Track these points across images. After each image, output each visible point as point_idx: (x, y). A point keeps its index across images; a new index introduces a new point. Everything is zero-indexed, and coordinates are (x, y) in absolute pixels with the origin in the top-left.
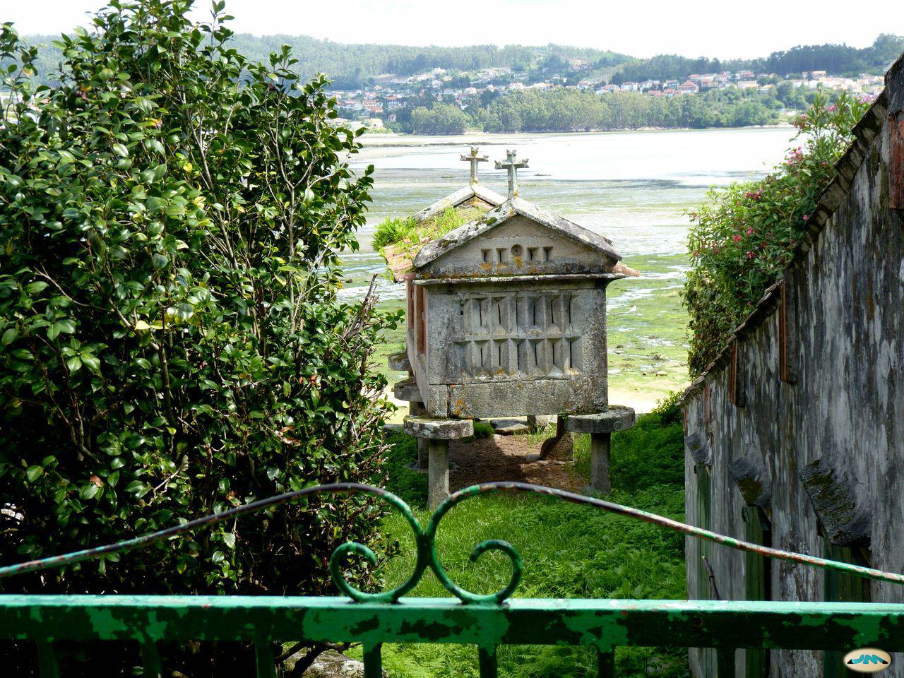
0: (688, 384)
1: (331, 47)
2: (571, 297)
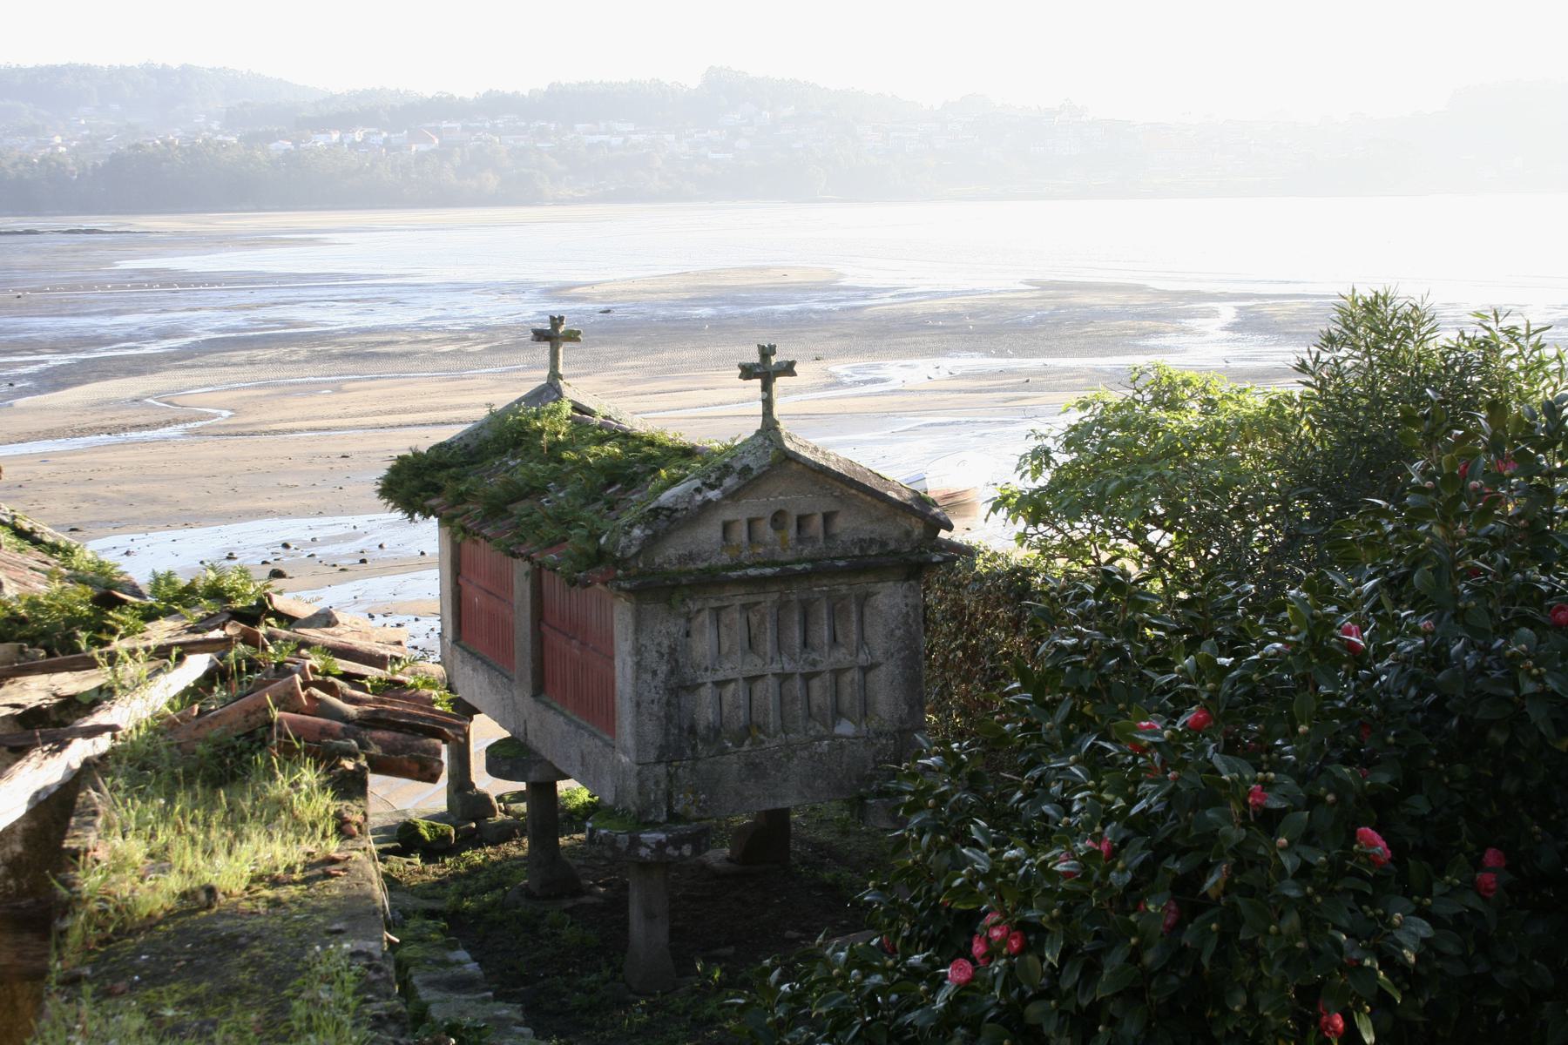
0: (89, 882)
1: (20, 70)
2: (868, 595)
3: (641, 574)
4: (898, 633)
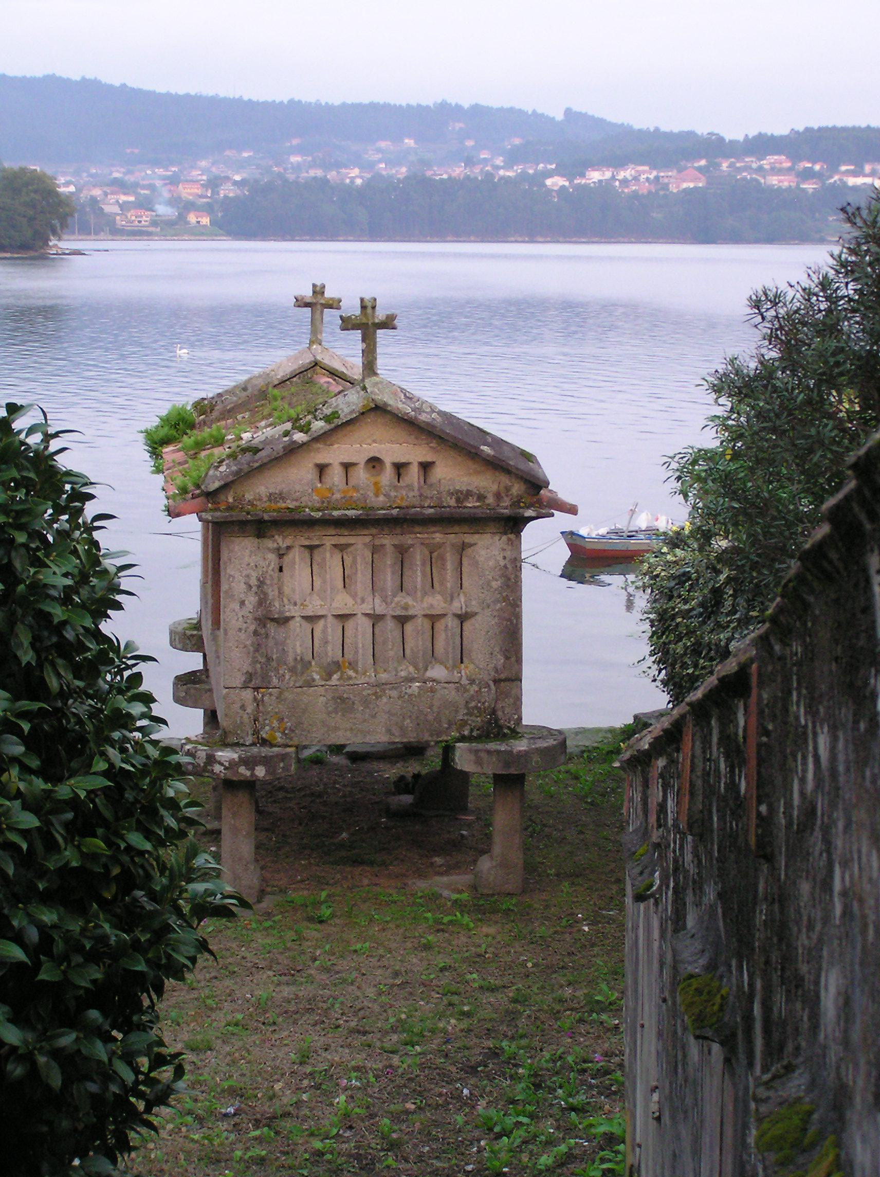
3: (230, 508)
4: (495, 584)
